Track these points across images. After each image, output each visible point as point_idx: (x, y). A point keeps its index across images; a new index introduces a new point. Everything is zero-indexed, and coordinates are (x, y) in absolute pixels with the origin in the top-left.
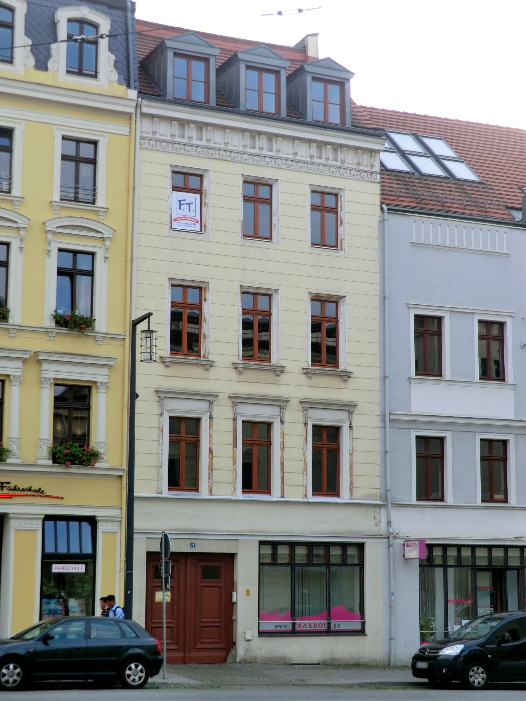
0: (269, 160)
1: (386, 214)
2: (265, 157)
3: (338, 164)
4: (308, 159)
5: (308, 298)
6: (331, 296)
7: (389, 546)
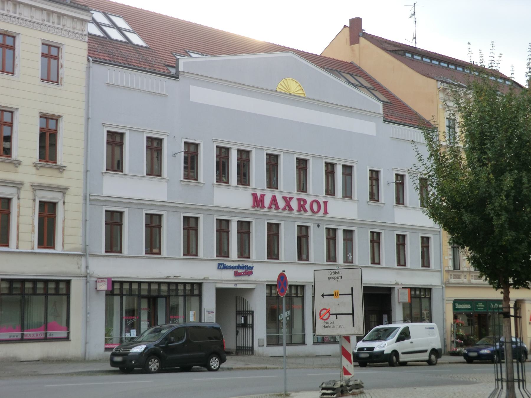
0: (14, 19)
1: (91, 63)
2: (11, 17)
3: (61, 27)
4: (41, 22)
5: (38, 116)
6: (53, 115)
7: (87, 282)
